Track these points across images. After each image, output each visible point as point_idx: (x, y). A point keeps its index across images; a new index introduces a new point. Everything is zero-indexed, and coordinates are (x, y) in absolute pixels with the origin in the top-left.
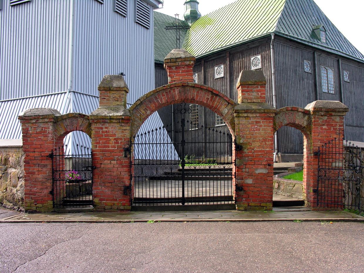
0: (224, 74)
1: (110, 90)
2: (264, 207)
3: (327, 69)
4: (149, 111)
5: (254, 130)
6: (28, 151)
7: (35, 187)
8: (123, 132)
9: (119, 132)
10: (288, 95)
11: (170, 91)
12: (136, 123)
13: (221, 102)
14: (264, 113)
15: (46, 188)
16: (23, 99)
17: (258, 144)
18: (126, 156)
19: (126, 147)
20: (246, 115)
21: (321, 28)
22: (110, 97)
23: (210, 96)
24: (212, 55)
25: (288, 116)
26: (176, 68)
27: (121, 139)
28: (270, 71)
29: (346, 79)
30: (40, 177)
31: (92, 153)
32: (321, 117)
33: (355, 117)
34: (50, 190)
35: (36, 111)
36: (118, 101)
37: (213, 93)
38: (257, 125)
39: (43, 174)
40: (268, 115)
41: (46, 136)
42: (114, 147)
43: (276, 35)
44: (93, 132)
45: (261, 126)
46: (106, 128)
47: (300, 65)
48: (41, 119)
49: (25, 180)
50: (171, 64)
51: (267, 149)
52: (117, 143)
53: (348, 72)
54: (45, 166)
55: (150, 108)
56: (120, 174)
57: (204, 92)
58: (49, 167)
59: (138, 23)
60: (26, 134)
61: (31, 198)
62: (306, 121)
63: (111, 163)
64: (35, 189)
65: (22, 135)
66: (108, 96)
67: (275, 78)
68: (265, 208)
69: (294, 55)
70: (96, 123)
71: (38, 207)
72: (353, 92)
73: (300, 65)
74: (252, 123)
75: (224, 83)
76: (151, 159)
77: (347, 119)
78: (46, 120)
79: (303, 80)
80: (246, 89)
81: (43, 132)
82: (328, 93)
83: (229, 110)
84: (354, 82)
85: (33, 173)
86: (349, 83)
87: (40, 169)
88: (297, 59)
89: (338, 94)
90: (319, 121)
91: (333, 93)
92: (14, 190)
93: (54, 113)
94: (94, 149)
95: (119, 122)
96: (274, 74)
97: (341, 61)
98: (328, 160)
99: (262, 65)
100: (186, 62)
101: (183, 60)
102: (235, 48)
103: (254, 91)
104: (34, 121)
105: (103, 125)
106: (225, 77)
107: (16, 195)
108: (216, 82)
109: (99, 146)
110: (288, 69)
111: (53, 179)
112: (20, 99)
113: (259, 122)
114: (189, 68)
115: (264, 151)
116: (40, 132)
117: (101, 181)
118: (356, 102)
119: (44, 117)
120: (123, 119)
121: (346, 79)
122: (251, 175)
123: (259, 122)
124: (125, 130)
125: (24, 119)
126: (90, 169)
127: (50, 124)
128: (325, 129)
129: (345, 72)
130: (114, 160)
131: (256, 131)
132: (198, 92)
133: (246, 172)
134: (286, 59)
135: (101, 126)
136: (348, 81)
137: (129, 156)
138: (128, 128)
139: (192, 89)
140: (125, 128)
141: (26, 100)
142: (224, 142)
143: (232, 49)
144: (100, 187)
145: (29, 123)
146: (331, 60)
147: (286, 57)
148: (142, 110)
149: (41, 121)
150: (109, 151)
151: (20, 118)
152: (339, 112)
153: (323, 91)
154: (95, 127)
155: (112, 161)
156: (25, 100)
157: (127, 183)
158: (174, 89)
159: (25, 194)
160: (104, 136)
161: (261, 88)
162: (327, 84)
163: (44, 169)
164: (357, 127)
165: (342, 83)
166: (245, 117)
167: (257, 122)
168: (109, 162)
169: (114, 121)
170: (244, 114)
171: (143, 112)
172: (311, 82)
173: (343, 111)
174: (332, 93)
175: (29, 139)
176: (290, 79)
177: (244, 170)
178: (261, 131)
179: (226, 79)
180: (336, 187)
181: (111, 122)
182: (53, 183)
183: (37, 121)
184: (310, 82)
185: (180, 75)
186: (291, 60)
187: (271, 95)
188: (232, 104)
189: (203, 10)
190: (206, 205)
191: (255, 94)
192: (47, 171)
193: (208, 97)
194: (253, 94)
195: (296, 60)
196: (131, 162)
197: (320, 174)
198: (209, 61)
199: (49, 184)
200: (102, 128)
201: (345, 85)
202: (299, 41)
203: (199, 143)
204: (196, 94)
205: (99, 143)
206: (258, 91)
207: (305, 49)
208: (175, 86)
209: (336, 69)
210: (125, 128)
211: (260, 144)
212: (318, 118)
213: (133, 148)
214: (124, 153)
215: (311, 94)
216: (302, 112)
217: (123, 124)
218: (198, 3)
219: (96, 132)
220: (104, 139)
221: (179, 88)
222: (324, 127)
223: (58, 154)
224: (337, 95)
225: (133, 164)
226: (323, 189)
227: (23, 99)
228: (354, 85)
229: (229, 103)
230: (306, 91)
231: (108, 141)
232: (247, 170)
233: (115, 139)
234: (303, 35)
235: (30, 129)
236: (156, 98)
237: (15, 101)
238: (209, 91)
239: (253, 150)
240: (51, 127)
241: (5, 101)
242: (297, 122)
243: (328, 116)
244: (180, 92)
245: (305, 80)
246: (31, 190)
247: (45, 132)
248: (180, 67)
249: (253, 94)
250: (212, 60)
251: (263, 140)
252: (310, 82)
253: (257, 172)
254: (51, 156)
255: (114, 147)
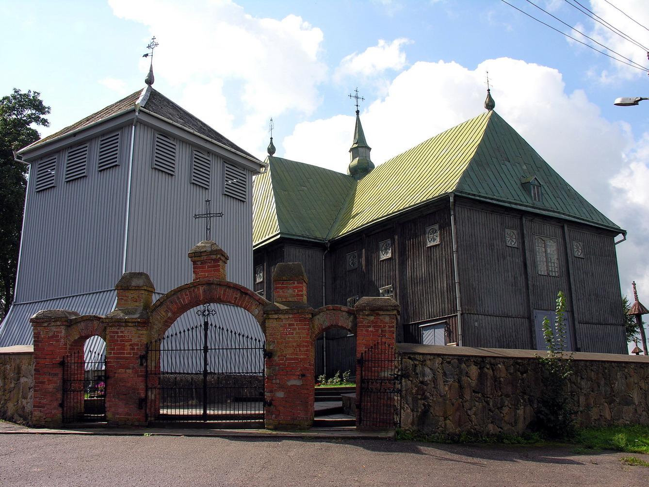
0: (392, 254)
1: (128, 289)
2: (297, 425)
3: (544, 241)
4: (170, 313)
5: (287, 334)
6: (39, 358)
7: (45, 398)
8: (139, 337)
9: (135, 336)
10: (479, 281)
11: (194, 290)
12: (155, 327)
13: (252, 301)
14: (298, 314)
15: (56, 399)
16: (73, 296)
17: (290, 351)
18: (142, 364)
19: (142, 354)
20: (276, 316)
21: (533, 182)
22: (128, 297)
23: (239, 294)
24: (375, 226)
25: (330, 317)
26: (202, 263)
27: (137, 345)
28: (452, 248)
29: (578, 253)
30: (50, 387)
31: (105, 360)
32: (366, 317)
33: (595, 310)
34: (60, 402)
35: (49, 314)
36: (136, 302)
37: (242, 292)
38: (290, 328)
39: (53, 384)
40: (303, 316)
41: (58, 341)
42: (130, 354)
43: (455, 196)
44: (108, 337)
45: (295, 329)
46: (122, 332)
47: (500, 236)
48: (53, 322)
49: (35, 391)
50: (196, 258)
51: (302, 357)
52: (133, 349)
53: (580, 243)
54: (55, 375)
55: (171, 310)
56: (135, 384)
57: (232, 290)
58: (60, 376)
59: (228, 196)
60: (38, 338)
61: (40, 411)
62: (351, 322)
63: (126, 372)
64: (44, 401)
65: (33, 339)
66: (126, 297)
67: (458, 258)
68: (298, 426)
69: (488, 222)
70: (110, 326)
71: (47, 422)
72: (590, 272)
73: (500, 236)
74: (284, 326)
75: (391, 266)
76: (224, 372)
77: (581, 313)
78: (58, 323)
79: (504, 258)
80: (280, 285)
81: (55, 337)
82: (548, 275)
83: (259, 311)
84: (592, 257)
85: (43, 383)
86: (584, 259)
87: (51, 379)
88: (494, 227)
89: (564, 275)
90: (364, 322)
91: (557, 275)
92: (24, 401)
93: (68, 316)
94: (108, 356)
95: (135, 326)
96: (457, 251)
97: (568, 227)
98: (374, 369)
99: (441, 239)
100: (212, 256)
101: (208, 254)
102: (404, 216)
103: (290, 288)
104: (46, 324)
105: (118, 329)
106: (394, 257)
107: (26, 408)
108: (381, 265)
109: (113, 353)
110: (479, 244)
111: (63, 390)
112: (70, 297)
113: (293, 325)
114: (215, 263)
115: (297, 359)
116: (52, 337)
117: (114, 393)
118: (596, 287)
119: (57, 319)
120: (138, 322)
121: (578, 253)
122: (282, 387)
123: (293, 325)
124: (142, 334)
125: (36, 322)
126: (103, 378)
127: (62, 327)
128: (372, 331)
129: (575, 243)
130: (130, 369)
131: (289, 336)
132: (225, 291)
133: (277, 384)
134: (476, 229)
135: (116, 330)
136: (582, 256)
137: (145, 364)
138: (145, 332)
139: (219, 287)
140: (141, 332)
141: (114, 293)
142: (180, 350)
143: (401, 217)
144: (113, 399)
145: (41, 326)
146: (550, 227)
147: (476, 227)
148: (162, 312)
149: (53, 324)
150: (124, 358)
151: (32, 320)
152: (388, 310)
153: (540, 273)
154: (110, 332)
155: (127, 370)
156: (75, 297)
157: (143, 396)
158: (199, 288)
159: (34, 406)
160: (119, 341)
161: (297, 284)
162: (545, 263)
163: (55, 379)
164: (599, 325)
165: (570, 259)
166: (276, 319)
167: (290, 325)
168: (123, 370)
169: (130, 324)
170: (274, 315)
171: (164, 314)
172: (519, 261)
173: (393, 310)
174: (554, 275)
175: (40, 344)
176: (483, 257)
177: (274, 381)
178: (294, 335)
179: (394, 261)
180: (385, 403)
181: (127, 326)
182: (63, 394)
183: (50, 324)
184: (517, 260)
185: (205, 271)
186: (484, 231)
187: (454, 282)
188: (263, 305)
189: (377, 158)
190: (238, 422)
191: (290, 291)
192: (58, 380)
193: (237, 296)
194: (288, 291)
195: (491, 229)
196: (147, 371)
197: (363, 385)
198: (372, 235)
199: (59, 396)
200: (117, 333)
201: (576, 263)
202: (495, 202)
203: (227, 349)
204: (222, 293)
205: (113, 349)
206: (294, 288)
207: (506, 213)
208: (199, 285)
209: (561, 240)
210: (141, 332)
211: (293, 351)
212: (363, 318)
213: (149, 355)
214: (140, 360)
215: (519, 278)
216: (346, 312)
217: (140, 328)
218: (370, 149)
219: (111, 337)
220: (119, 345)
221: (204, 287)
222: (370, 329)
223: (73, 362)
224: (562, 278)
225: (149, 374)
226: (369, 404)
227: (73, 296)
228: (591, 261)
229: (260, 303)
230: (510, 273)
231: (123, 347)
232: (278, 381)
233: (131, 345)
234: (507, 193)
235: (41, 333)
236: (178, 298)
237: (95, 295)
238: (238, 289)
239: (285, 358)
240: (63, 331)
241: (54, 299)
242: (340, 324)
243: (375, 316)
244: (204, 291)
245: (508, 258)
246: (40, 403)
247: (57, 336)
248: (206, 263)
249: (288, 291)
250: (375, 234)
251: (297, 345)
252: (517, 260)
253: (290, 383)
254: (62, 364)
255: (130, 354)
